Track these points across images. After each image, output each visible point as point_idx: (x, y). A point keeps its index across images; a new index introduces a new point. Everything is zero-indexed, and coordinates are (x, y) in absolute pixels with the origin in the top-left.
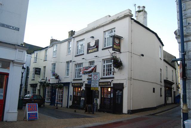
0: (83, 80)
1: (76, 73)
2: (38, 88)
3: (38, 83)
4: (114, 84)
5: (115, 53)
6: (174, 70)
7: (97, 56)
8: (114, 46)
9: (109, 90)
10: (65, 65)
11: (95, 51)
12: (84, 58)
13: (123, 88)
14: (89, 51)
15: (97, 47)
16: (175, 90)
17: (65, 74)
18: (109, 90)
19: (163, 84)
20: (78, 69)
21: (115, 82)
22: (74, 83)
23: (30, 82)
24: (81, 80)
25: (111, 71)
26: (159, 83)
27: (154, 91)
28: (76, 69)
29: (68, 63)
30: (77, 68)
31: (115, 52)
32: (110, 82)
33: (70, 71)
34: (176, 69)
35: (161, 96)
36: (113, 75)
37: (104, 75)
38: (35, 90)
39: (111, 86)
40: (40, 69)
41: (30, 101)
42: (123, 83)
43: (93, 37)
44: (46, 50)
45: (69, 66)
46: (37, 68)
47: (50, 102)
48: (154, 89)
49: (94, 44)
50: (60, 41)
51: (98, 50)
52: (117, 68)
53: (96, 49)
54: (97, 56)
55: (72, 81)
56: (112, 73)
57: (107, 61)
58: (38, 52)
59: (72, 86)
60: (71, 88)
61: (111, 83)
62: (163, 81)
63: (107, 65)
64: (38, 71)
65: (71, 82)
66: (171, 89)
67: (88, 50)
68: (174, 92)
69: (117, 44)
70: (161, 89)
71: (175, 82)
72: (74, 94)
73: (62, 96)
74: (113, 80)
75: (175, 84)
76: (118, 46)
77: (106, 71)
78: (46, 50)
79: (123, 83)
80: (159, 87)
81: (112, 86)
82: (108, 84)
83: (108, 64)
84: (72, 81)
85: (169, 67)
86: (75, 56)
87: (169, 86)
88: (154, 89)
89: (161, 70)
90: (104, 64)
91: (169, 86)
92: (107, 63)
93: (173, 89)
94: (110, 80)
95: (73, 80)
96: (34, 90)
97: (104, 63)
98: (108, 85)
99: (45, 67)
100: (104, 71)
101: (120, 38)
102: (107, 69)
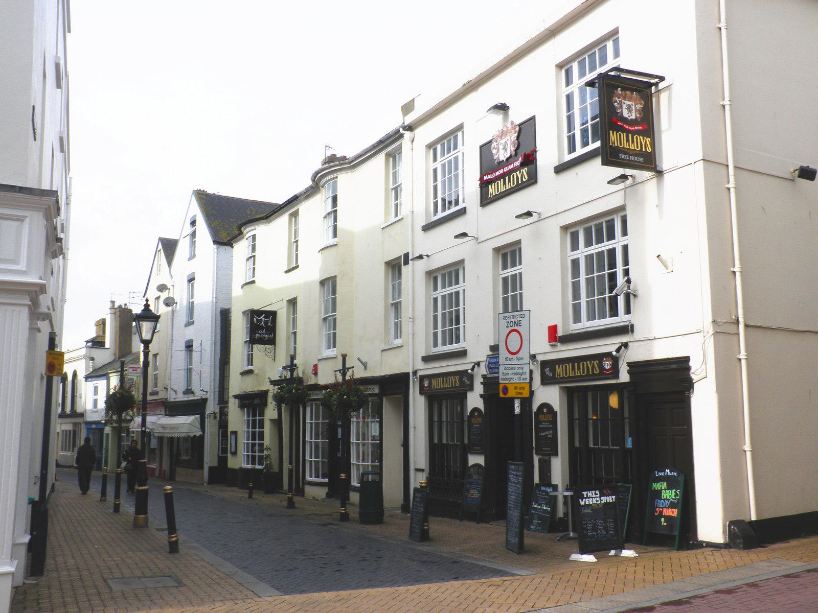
0: (472, 358)
1: (435, 318)
2: (271, 412)
3: (266, 386)
4: (632, 365)
5: (624, 177)
7: (529, 214)
9: (614, 401)
10: (379, 276)
12: (464, 235)
13: (687, 385)
14: (492, 190)
15: (530, 160)
17: (387, 332)
18: (614, 401)
20: (444, 297)
21: (637, 353)
22: (430, 377)
23: (237, 385)
24: (463, 354)
25: (613, 286)
28: (436, 300)
29: (395, 267)
30: (441, 292)
31: (628, 172)
32: (608, 355)
33: (406, 311)
36: (628, 311)
37: (436, 345)
38: (262, 425)
40: (273, 314)
41: (120, 416)
42: (686, 360)
43: (502, 108)
46: (258, 313)
47: (326, 480)
49: (511, 149)
50: (344, 158)
51: (533, 179)
52: (132, 397)
53: (524, 170)
54: (529, 214)
55: (420, 365)
56: (621, 300)
57: (588, 232)
58: (261, 231)
59: (422, 391)
60: (418, 405)
61: (615, 361)
63: (589, 258)
64: (262, 328)
65: (415, 373)
67: (484, 185)
69: (633, 122)
72: (436, 441)
73: (378, 450)
74: (626, 345)
76: (639, 133)
77: (590, 293)
78: (295, 215)
79: (686, 360)
81: (624, 377)
82: (601, 366)
83: (595, 249)
84: (420, 365)
86: (427, 228)
92: (588, 243)
94: (609, 345)
95: (427, 359)
96: (254, 421)
97: (575, 247)
98: (603, 374)
99: (293, 302)
100: (576, 295)
101: (650, 85)
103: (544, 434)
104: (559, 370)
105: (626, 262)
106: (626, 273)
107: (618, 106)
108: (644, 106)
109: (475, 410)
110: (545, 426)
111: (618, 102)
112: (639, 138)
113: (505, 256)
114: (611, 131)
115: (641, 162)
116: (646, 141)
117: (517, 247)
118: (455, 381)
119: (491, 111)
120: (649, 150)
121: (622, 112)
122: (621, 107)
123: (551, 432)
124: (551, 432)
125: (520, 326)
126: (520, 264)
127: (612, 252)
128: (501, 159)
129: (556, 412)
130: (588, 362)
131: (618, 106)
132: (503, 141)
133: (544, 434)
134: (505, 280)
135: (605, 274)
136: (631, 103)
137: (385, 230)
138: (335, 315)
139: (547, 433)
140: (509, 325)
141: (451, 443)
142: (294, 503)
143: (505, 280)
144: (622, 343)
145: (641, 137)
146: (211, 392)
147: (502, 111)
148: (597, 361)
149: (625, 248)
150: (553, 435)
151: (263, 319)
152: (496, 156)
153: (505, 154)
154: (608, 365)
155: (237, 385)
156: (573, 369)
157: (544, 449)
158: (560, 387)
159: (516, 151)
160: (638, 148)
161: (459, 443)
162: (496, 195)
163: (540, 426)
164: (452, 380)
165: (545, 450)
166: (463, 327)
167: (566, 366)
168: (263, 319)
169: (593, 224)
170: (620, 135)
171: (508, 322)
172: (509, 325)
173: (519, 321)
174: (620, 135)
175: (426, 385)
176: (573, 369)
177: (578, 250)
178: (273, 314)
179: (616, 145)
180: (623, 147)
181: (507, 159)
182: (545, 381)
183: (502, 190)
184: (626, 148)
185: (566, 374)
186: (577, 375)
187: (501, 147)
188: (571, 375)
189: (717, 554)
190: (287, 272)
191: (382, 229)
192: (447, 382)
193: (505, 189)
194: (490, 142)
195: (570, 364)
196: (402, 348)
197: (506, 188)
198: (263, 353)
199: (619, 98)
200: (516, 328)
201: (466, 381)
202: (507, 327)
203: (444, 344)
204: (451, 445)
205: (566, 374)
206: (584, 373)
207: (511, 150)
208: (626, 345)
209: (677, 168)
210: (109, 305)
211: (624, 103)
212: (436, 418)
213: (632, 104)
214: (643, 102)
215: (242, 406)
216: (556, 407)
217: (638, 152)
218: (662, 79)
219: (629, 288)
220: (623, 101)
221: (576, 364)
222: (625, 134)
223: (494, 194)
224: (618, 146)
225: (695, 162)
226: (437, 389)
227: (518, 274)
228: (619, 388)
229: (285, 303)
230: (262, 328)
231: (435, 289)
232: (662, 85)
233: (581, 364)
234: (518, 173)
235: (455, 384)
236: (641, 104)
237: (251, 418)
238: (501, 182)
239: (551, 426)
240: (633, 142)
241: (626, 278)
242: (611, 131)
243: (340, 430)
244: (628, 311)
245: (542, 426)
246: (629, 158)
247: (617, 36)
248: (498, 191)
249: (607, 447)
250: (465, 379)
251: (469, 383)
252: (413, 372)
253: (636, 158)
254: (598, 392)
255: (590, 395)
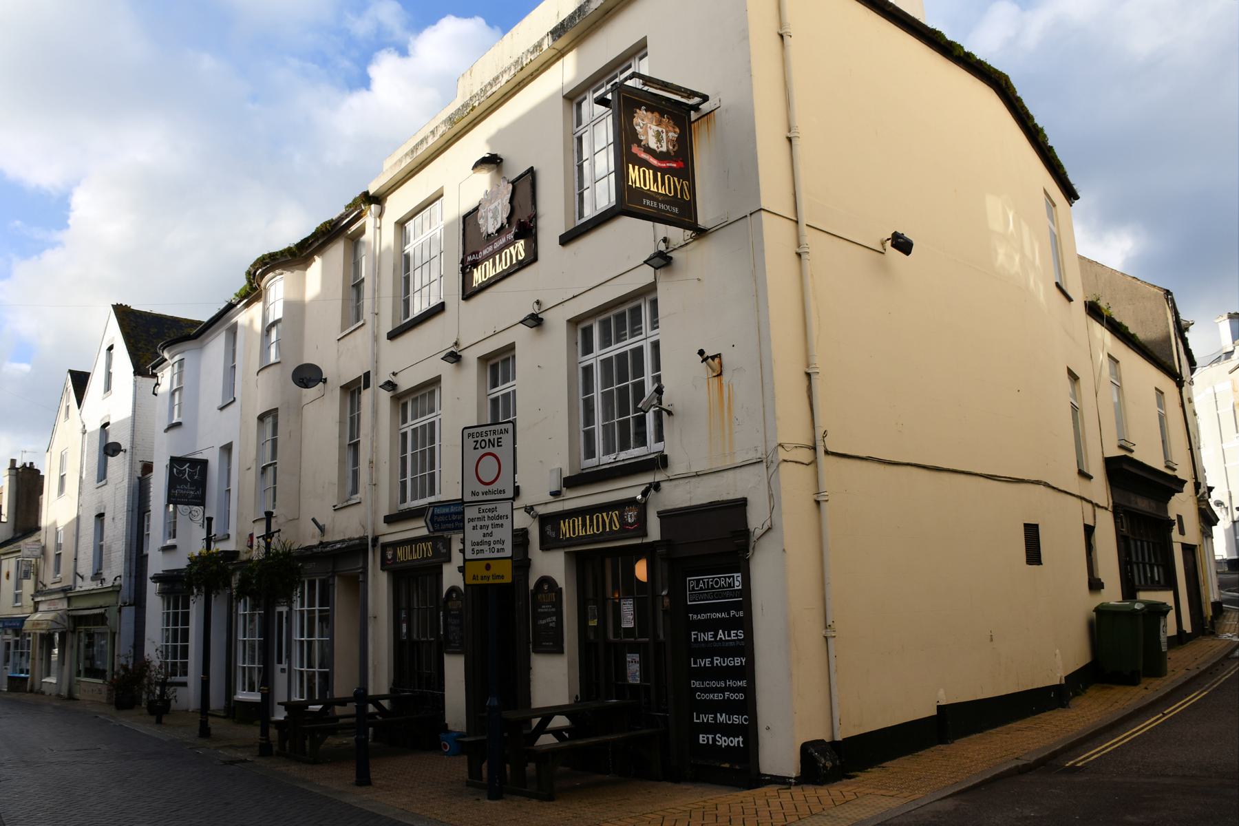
1: (404, 460)
4: (664, 516)
6: (1168, 385)
8: (634, 173)
9: (641, 570)
11: (522, 265)
14: (478, 276)
16: (1192, 534)
18: (641, 570)
19: (1099, 489)
20: (415, 431)
21: (677, 496)
22: (395, 545)
23: (157, 564)
26: (1073, 483)
27: (1034, 555)
28: (404, 435)
32: (632, 502)
34: (1180, 383)
35: (583, 470)
37: (590, 453)
39: (645, 535)
40: (204, 463)
44: (228, 330)
45: (359, 415)
48: (1032, 533)
53: (521, 244)
57: (605, 326)
59: (384, 565)
60: (379, 587)
61: (641, 507)
62: (1097, 469)
63: (606, 363)
65: (375, 539)
66: (1163, 526)
67: (468, 266)
68: (1189, 550)
70: (1089, 531)
71: (1183, 472)
74: (656, 486)
75: (1189, 488)
80: (1072, 516)
81: (654, 531)
83: (614, 350)
85: (1132, 362)
86: (393, 336)
87: (1143, 504)
88: (1032, 533)
89: (1073, 377)
90: (590, 359)
91: (1143, 504)
92: (606, 343)
93: (1176, 528)
94: (631, 489)
95: (389, 520)
97: (588, 349)
98: (625, 531)
99: (227, 449)
102: (607, 397)
103: (544, 622)
104: (565, 527)
105: (657, 366)
106: (657, 379)
107: (641, 130)
108: (679, 135)
109: (453, 589)
110: (546, 610)
111: (642, 125)
112: (672, 178)
113: (494, 368)
114: (630, 166)
115: (675, 214)
116: (682, 184)
117: (510, 355)
118: (427, 549)
119: (479, 167)
120: (687, 198)
121: (647, 139)
122: (646, 133)
123: (554, 619)
124: (554, 619)
125: (498, 446)
126: (514, 378)
127: (638, 352)
128: (490, 232)
129: (561, 588)
130: (604, 514)
131: (641, 130)
132: (492, 207)
133: (544, 622)
134: (495, 401)
135: (628, 386)
136: (660, 130)
137: (342, 341)
138: (276, 463)
139: (549, 620)
140: (478, 446)
141: (422, 639)
142: (209, 729)
143: (495, 401)
144: (650, 484)
145: (676, 179)
146: (125, 576)
147: (493, 165)
148: (617, 512)
149: (656, 346)
150: (556, 622)
151: (187, 469)
152: (484, 228)
153: (496, 223)
154: (631, 517)
155: (157, 564)
156: (584, 525)
157: (544, 644)
158: (565, 553)
159: (509, 218)
160: (670, 193)
161: (433, 639)
162: (483, 282)
163: (539, 610)
164: (423, 549)
165: (546, 646)
166: (438, 472)
167: (574, 521)
168: (187, 469)
169: (611, 314)
170: (644, 172)
171: (477, 441)
172: (478, 446)
173: (498, 439)
174: (644, 172)
175: (389, 557)
176: (584, 525)
177: (593, 352)
178: (204, 463)
179: (638, 185)
180: (649, 190)
181: (498, 231)
182: (546, 545)
183: (491, 275)
184: (653, 192)
185: (574, 534)
186: (588, 533)
187: (490, 215)
188: (581, 534)
189: (785, 795)
190: (222, 409)
191: (338, 340)
192: (416, 551)
193: (494, 273)
194: (476, 209)
195: (580, 518)
196: (360, 505)
197: (495, 271)
198: (188, 517)
199: (643, 120)
200: (491, 450)
201: (441, 548)
202: (475, 448)
203: (414, 498)
204: (423, 642)
205: (574, 534)
206: (598, 530)
207: (502, 218)
208: (656, 486)
209: (726, 224)
210: (8, 465)
211: (650, 128)
212: (404, 605)
213: (662, 131)
214: (677, 130)
215: (163, 593)
216: (561, 581)
217: (669, 198)
218: (705, 98)
219: (660, 403)
220: (649, 125)
221: (588, 517)
222: (651, 171)
223: (480, 281)
224: (641, 188)
225: (751, 214)
226: (403, 562)
227: (511, 392)
228: (647, 551)
229: (217, 451)
230: (185, 482)
231: (404, 421)
232: (705, 107)
233: (595, 517)
234: (512, 248)
235: (427, 554)
236: (675, 132)
237: (171, 611)
238: (489, 264)
239: (554, 610)
240: (663, 183)
241: (656, 385)
242: (630, 166)
243: (404, 626)
244: (660, 437)
245: (542, 610)
246: (658, 205)
247: (639, 326)
248: (485, 277)
249: (425, 639)
250: (440, 546)
251: (445, 551)
252: (372, 539)
253: (668, 207)
254: (620, 558)
255: (608, 562)
